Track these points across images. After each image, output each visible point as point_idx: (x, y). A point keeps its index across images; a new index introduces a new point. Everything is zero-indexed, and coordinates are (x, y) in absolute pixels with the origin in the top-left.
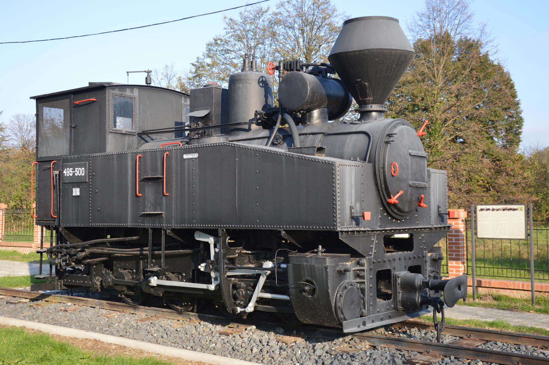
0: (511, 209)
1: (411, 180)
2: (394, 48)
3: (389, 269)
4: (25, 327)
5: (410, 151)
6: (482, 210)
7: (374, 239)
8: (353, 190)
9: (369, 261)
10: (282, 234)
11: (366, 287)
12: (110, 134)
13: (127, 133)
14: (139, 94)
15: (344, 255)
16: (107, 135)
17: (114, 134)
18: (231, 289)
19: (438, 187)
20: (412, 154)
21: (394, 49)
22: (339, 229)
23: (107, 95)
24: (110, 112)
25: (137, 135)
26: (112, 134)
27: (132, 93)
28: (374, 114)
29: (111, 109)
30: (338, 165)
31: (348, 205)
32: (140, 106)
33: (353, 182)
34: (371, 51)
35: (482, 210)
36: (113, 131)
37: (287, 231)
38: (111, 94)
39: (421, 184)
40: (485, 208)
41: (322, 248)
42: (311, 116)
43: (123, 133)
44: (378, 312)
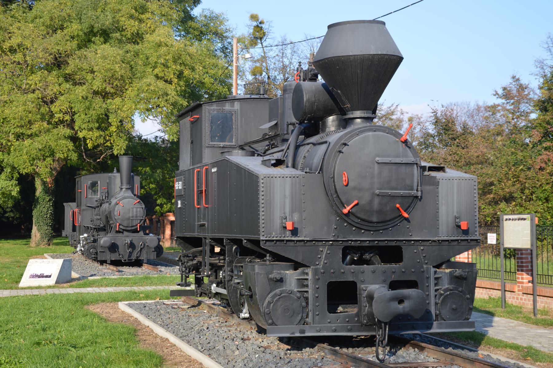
0: (522, 219)
1: (378, 189)
2: (351, 54)
3: (353, 282)
4: (148, 327)
5: (377, 159)
6: (506, 220)
7: (325, 250)
8: (288, 202)
9: (316, 272)
10: (243, 243)
11: (310, 295)
12: (206, 149)
13: (225, 146)
14: (241, 107)
15: (283, 263)
16: (203, 150)
17: (211, 148)
18: (238, 296)
19: (455, 195)
20: (379, 162)
21: (351, 55)
22: (262, 238)
23: (203, 112)
24: (207, 128)
25: (238, 148)
26: (208, 148)
27: (233, 106)
28: (359, 120)
29: (207, 125)
30: (262, 178)
31: (277, 214)
32: (241, 119)
33: (288, 193)
34: (330, 59)
35: (506, 220)
36: (210, 146)
37: (249, 240)
38: (207, 110)
39: (401, 192)
40: (511, 219)
41: (269, 256)
42: (324, 125)
43: (220, 147)
44: (330, 322)
